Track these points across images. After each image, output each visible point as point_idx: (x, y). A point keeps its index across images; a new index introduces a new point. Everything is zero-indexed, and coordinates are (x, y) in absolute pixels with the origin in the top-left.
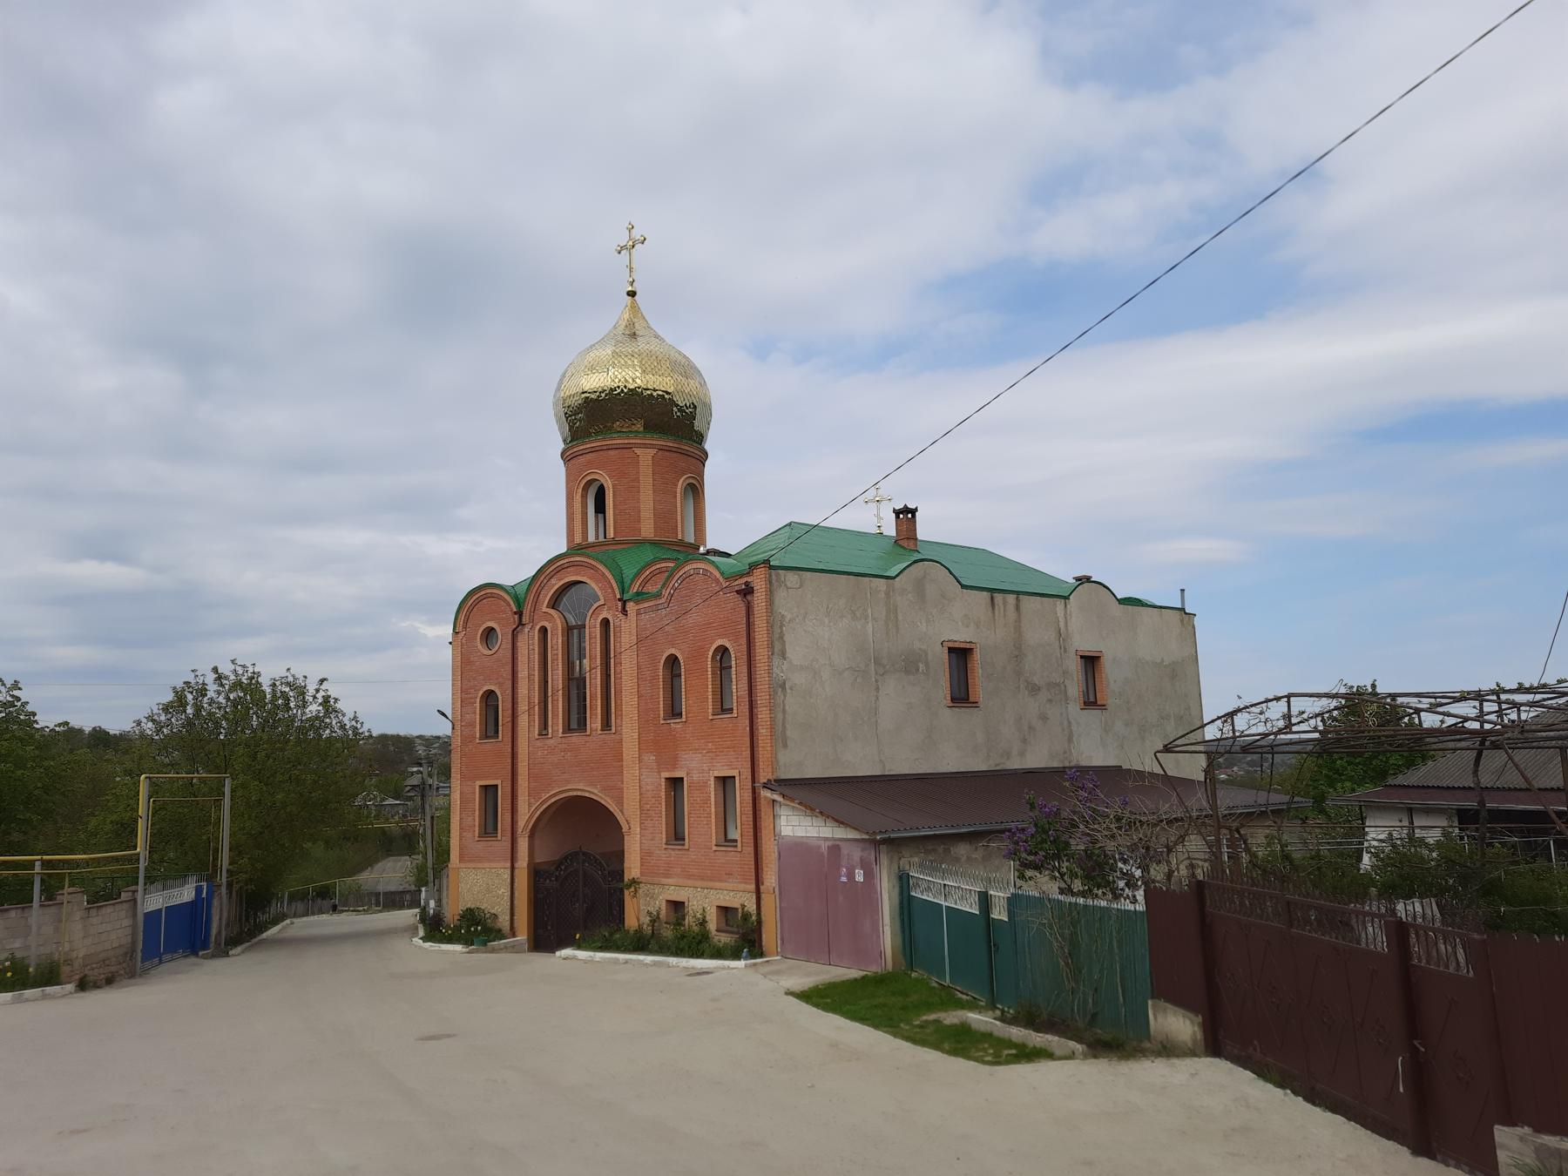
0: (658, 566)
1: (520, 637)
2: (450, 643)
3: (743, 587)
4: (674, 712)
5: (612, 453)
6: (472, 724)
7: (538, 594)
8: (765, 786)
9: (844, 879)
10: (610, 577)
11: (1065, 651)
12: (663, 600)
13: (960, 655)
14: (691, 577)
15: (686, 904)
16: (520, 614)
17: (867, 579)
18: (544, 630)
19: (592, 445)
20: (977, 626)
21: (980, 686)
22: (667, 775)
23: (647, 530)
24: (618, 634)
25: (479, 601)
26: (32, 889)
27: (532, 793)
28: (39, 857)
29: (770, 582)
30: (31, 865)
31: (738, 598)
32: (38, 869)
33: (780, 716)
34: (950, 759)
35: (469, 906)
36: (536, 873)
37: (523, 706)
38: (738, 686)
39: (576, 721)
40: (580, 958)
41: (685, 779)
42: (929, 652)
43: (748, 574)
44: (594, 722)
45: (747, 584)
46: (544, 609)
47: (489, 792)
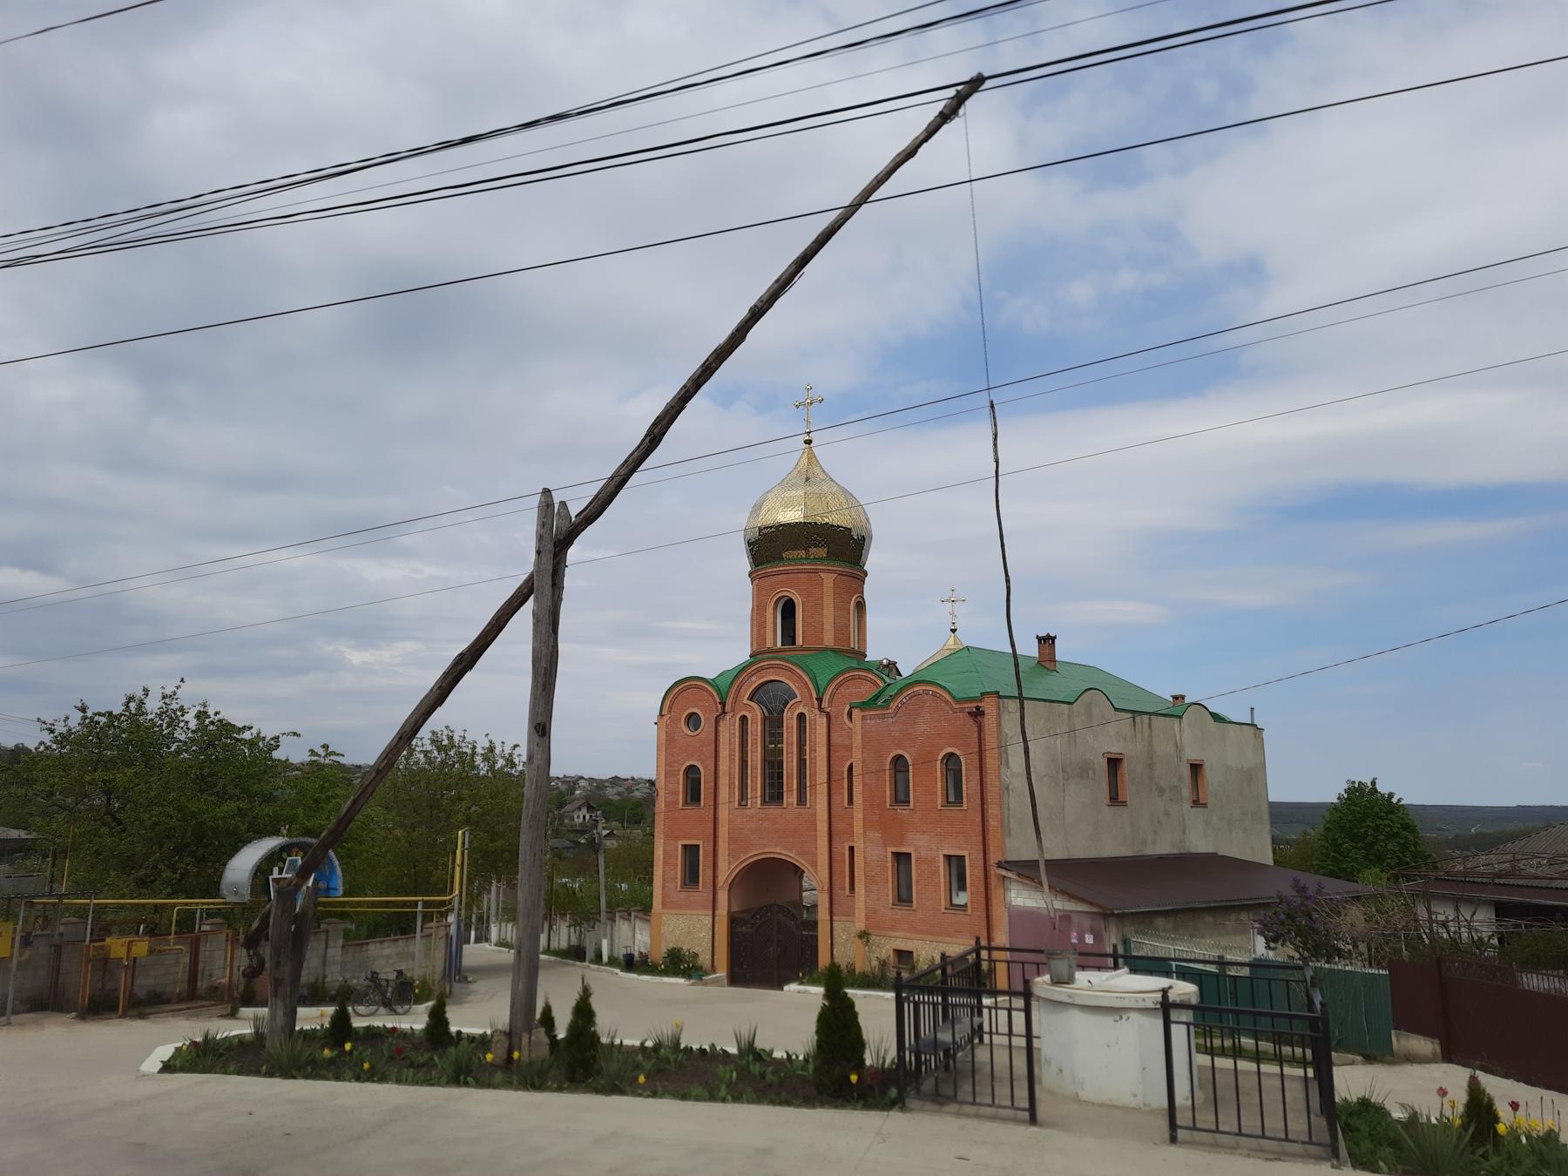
0: (851, 674)
1: (721, 723)
2: (656, 723)
3: (974, 710)
4: (900, 798)
6: (676, 793)
8: (999, 865)
9: (1074, 941)
10: (807, 679)
11: (1181, 760)
12: (890, 711)
13: (1114, 763)
15: (915, 955)
16: (723, 704)
17: (1056, 705)
18: (744, 719)
19: (785, 568)
20: (1125, 740)
21: (1128, 790)
22: (894, 850)
23: (829, 640)
24: (813, 727)
25: (683, 690)
26: (416, 925)
27: (732, 854)
28: (421, 898)
29: (999, 709)
30: (416, 903)
31: (971, 722)
32: (420, 908)
33: (1006, 812)
34: (1111, 847)
35: (671, 946)
36: (733, 920)
37: (724, 781)
38: (969, 786)
39: (774, 793)
40: (813, 992)
41: (913, 856)
42: (1096, 762)
43: (980, 701)
44: (790, 798)
45: (978, 708)
46: (745, 701)
47: (691, 852)
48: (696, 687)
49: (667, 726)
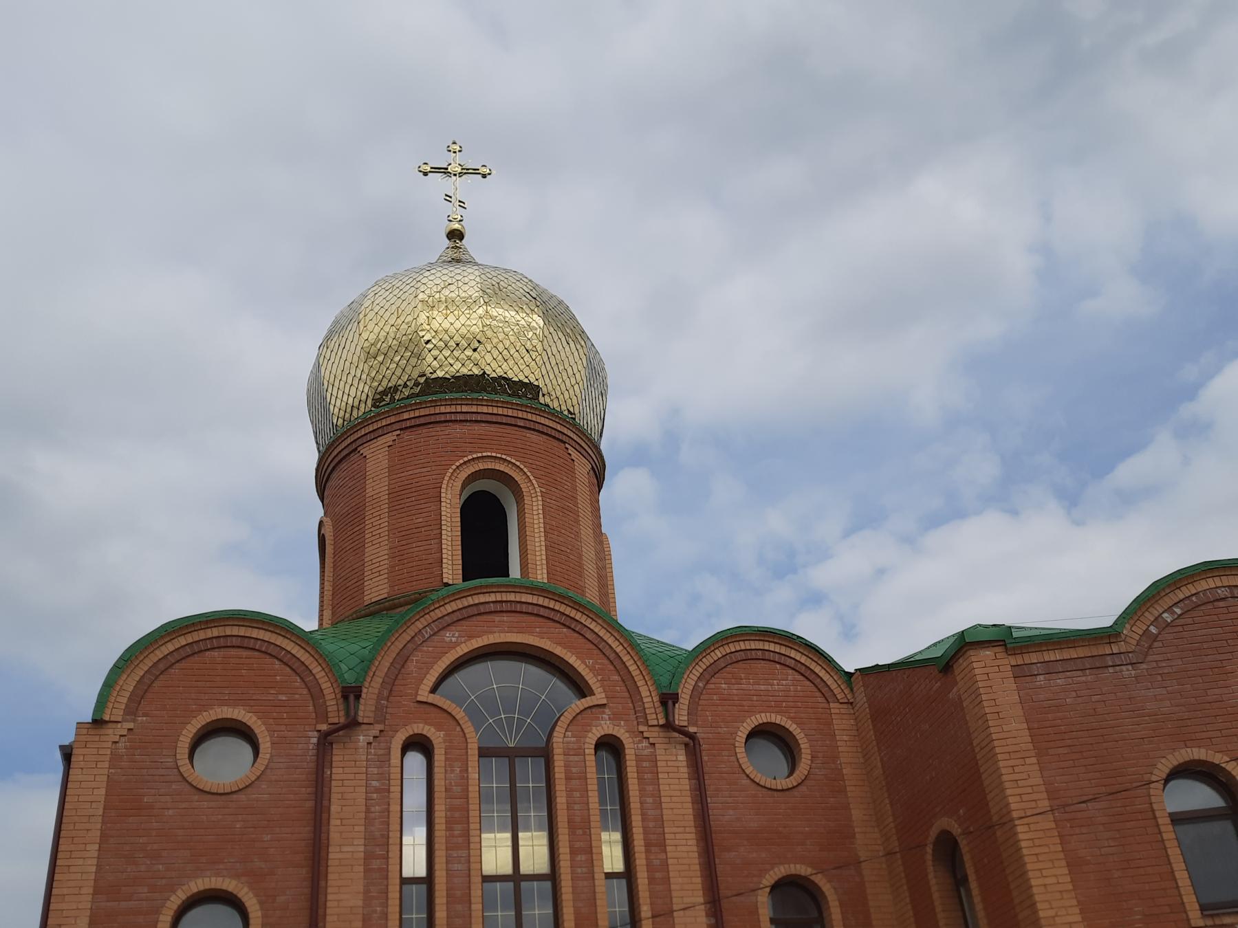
1: (338, 755)
5: (534, 437)
7: (402, 660)
14: (1222, 604)
16: (351, 694)
25: (196, 650)
46: (424, 694)
48: (244, 644)
49: (115, 758)
